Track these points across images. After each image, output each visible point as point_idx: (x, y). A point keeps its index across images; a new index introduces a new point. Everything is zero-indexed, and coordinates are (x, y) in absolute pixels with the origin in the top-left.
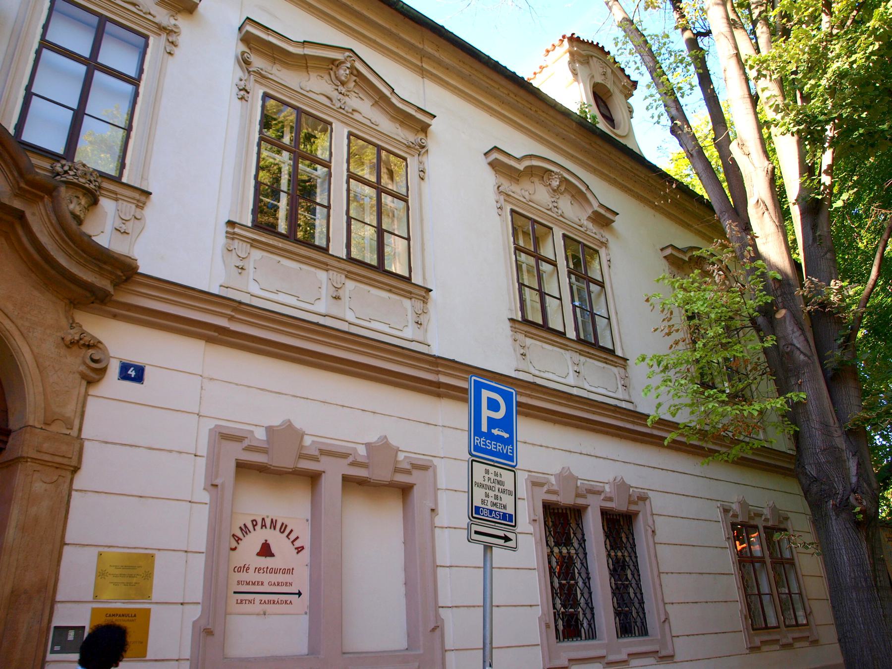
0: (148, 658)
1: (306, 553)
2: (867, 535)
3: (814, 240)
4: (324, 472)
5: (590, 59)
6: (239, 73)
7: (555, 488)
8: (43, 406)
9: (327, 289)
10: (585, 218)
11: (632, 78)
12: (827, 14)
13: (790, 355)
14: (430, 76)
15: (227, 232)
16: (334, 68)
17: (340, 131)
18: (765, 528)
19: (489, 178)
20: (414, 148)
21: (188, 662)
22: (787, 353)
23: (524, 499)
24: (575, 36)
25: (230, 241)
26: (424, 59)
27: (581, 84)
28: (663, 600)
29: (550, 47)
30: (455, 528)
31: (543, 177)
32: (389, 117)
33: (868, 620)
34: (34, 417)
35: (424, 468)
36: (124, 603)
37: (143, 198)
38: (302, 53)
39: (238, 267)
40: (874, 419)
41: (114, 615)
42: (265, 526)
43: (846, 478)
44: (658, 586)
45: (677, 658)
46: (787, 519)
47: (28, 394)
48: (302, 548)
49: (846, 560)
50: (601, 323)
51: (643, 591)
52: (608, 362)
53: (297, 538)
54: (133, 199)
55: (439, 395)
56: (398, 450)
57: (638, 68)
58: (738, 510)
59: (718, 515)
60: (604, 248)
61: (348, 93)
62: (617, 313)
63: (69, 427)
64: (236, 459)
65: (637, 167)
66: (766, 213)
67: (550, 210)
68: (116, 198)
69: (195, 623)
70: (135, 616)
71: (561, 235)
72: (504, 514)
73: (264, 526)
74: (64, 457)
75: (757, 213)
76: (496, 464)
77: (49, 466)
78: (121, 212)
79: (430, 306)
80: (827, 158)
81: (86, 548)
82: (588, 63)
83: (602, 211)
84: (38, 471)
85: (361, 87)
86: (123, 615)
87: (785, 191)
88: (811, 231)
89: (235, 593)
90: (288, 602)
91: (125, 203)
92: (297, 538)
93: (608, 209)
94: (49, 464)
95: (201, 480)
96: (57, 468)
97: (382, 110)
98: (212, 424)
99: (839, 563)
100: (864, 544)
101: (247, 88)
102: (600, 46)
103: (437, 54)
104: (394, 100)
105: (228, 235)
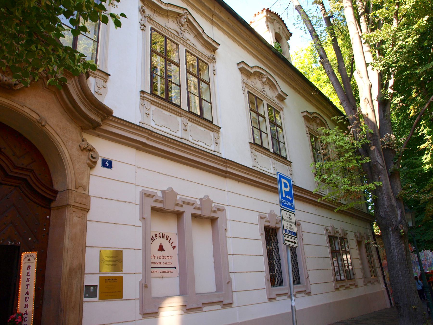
0: (123, 299)
1: (177, 249)
2: (404, 241)
3: (384, 117)
4: (185, 212)
5: (274, 20)
6: (140, 17)
7: (268, 219)
8: (74, 180)
9: (181, 125)
10: (275, 97)
11: (290, 32)
12: (396, 19)
13: (376, 166)
14: (215, 25)
15: (141, 96)
16: (179, 17)
17: (182, 49)
18: (340, 238)
19: (239, 76)
20: (211, 59)
21: (139, 300)
22: (375, 165)
23: (257, 224)
24: (269, 9)
25: (142, 100)
26: (214, 16)
27: (271, 33)
28: (307, 269)
29: (257, 13)
30: (234, 237)
31: (259, 77)
32: (201, 43)
33: (404, 276)
34: (71, 186)
35: (221, 210)
36: (112, 274)
37: (106, 77)
38: (167, 9)
39: (146, 113)
40: (407, 194)
41: (108, 280)
42: (160, 237)
43: (396, 218)
44: (305, 263)
45: (312, 294)
46: (347, 234)
47: (68, 174)
48: (175, 247)
49: (396, 251)
50: (281, 145)
51: (298, 265)
52: (285, 163)
53: (173, 242)
54: (103, 77)
55: (226, 177)
56: (212, 202)
57: (305, 31)
58: (331, 230)
59: (324, 232)
60: (282, 111)
61: (185, 31)
62: (287, 141)
63: (85, 190)
64: (151, 206)
65: (294, 74)
66: (368, 104)
67: (262, 92)
68: (95, 76)
69: (140, 282)
70: (117, 280)
71: (266, 104)
72: (293, 232)
73: (160, 237)
74: (84, 204)
75: (365, 104)
76: (289, 211)
77: (79, 209)
78: (98, 84)
79: (220, 135)
80: (391, 82)
81: (95, 248)
82: (273, 22)
83: (282, 94)
84: (75, 212)
85: (190, 28)
86: (112, 279)
87: (358, 91)
88: (383, 113)
89: (152, 268)
90: (171, 272)
91: (99, 79)
92: (173, 242)
93: (284, 93)
94: (79, 208)
95: (138, 216)
96: (82, 210)
97: (198, 40)
98: (140, 189)
99: (393, 253)
100: (403, 245)
101: (145, 24)
102: (278, 15)
103: (220, 14)
104: (204, 36)
105: (141, 98)
